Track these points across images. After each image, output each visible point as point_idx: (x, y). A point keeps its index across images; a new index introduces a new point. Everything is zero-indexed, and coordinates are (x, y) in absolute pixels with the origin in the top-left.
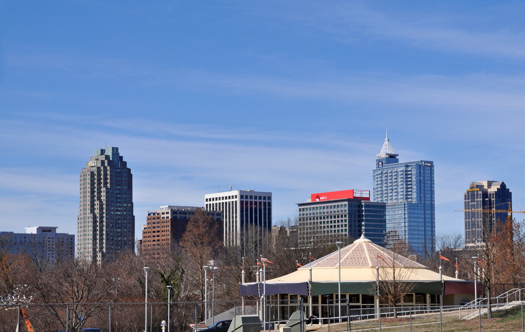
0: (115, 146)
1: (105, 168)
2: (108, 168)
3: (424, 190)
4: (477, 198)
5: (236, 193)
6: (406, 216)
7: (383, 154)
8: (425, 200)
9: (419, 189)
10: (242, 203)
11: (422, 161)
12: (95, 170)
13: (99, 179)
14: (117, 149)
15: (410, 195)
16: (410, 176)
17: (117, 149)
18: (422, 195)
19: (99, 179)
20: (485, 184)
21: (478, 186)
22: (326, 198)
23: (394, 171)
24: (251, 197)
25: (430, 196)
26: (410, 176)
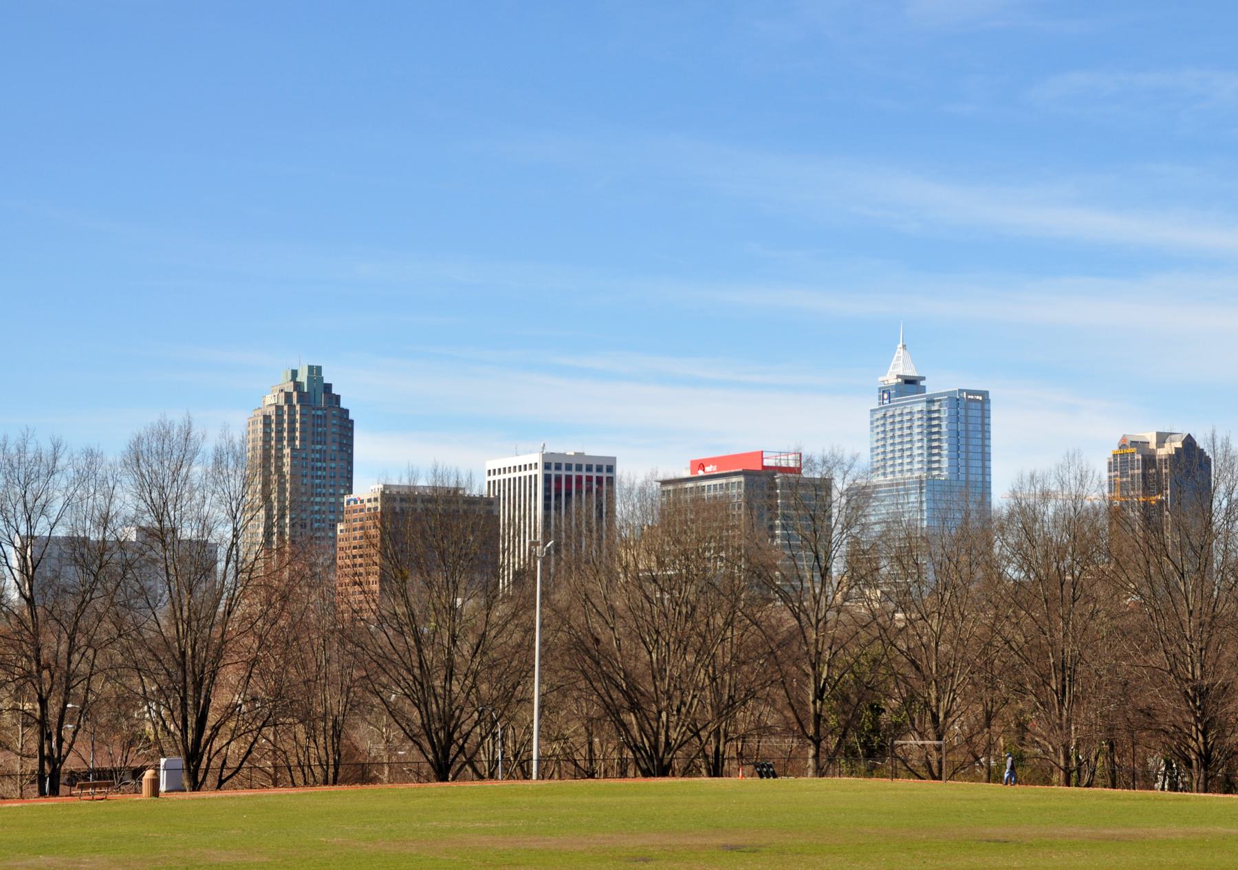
0: (315, 364)
1: (291, 407)
2: (298, 408)
3: (967, 452)
4: (1132, 469)
5: (536, 458)
6: (925, 507)
7: (891, 379)
8: (967, 474)
9: (956, 448)
10: (547, 479)
11: (961, 391)
12: (271, 411)
13: (280, 432)
14: (319, 369)
15: (935, 462)
16: (936, 422)
17: (319, 369)
18: (962, 463)
19: (280, 432)
20: (1152, 439)
21: (1134, 444)
22: (715, 468)
23: (906, 411)
24: (579, 468)
25: (980, 464)
26: (936, 422)
